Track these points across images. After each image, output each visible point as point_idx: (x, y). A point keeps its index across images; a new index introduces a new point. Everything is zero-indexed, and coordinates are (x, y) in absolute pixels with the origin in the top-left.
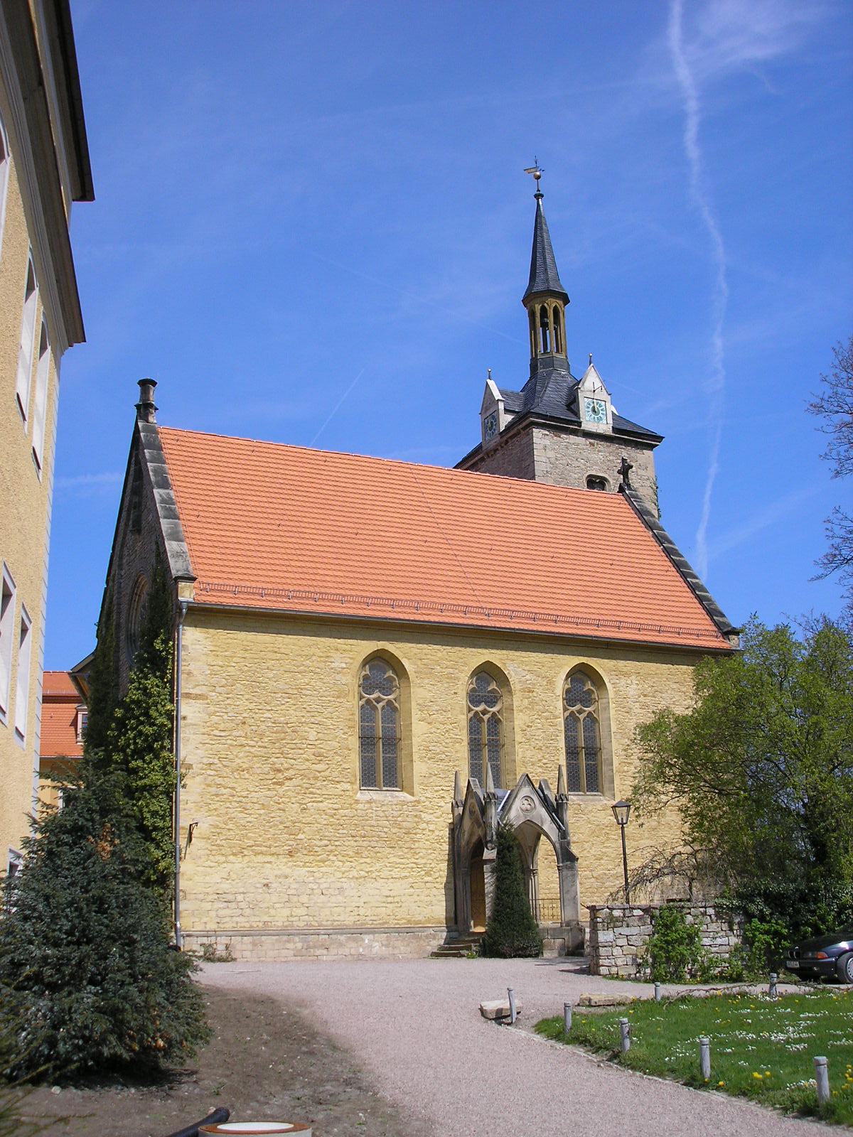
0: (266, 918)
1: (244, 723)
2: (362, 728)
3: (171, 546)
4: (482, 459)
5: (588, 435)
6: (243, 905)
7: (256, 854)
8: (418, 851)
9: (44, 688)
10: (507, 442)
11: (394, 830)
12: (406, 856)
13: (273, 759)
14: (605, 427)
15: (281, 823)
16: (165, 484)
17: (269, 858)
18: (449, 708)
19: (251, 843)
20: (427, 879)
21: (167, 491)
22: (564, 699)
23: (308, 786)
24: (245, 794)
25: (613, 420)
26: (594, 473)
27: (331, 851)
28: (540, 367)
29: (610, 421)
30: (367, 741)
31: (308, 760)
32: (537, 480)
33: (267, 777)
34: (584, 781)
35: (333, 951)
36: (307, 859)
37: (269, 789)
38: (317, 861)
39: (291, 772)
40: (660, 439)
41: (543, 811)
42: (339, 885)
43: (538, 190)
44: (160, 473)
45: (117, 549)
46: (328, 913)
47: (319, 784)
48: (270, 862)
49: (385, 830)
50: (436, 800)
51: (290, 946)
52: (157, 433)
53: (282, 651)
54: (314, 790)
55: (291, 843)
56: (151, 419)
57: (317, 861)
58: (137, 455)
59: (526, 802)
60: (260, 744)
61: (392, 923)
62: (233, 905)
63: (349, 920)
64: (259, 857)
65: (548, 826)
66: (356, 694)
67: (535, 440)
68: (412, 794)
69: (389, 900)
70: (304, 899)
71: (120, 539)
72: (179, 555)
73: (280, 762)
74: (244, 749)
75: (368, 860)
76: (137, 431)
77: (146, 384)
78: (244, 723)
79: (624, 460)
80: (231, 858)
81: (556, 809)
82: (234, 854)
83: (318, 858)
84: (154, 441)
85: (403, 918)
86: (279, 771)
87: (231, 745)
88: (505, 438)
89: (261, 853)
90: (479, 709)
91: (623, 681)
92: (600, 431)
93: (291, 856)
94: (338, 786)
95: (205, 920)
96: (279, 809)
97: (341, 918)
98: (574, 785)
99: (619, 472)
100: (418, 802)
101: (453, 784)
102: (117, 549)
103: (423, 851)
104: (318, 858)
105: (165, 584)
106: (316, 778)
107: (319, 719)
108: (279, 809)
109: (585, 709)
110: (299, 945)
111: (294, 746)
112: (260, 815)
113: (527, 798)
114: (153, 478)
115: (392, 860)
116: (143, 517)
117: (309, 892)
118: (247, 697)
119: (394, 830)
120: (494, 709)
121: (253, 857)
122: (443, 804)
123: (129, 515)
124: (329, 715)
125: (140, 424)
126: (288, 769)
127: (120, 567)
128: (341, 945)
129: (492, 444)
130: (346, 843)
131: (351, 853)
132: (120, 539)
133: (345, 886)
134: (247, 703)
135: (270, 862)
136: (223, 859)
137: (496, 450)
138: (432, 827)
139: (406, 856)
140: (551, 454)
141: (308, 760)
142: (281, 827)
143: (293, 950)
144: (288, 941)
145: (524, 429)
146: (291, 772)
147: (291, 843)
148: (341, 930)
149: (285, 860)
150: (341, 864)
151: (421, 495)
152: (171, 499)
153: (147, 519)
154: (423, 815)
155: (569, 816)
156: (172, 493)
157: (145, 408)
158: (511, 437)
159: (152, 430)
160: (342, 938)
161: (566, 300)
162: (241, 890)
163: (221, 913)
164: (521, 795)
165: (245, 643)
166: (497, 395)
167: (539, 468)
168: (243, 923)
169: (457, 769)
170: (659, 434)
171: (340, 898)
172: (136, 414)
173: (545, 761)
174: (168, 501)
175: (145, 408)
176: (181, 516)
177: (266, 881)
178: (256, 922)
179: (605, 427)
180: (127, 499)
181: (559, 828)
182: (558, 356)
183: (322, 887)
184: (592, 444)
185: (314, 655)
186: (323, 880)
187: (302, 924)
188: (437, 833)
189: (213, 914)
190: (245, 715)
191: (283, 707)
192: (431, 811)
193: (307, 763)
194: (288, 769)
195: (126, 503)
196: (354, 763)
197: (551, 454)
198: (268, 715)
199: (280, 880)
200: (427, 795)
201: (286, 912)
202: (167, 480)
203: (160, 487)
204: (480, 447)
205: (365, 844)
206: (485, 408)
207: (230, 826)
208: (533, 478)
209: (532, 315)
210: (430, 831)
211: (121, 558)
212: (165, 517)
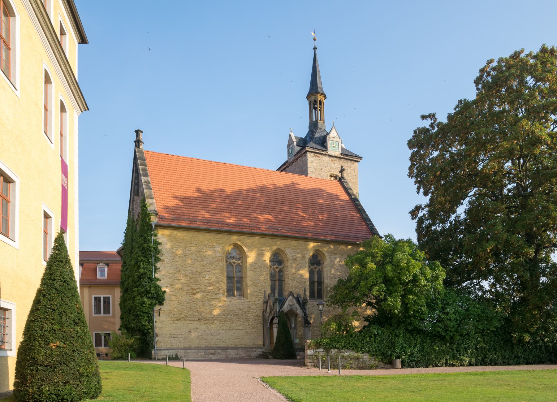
0: (190, 344)
1: (180, 271)
2: (227, 272)
3: (148, 201)
4: (287, 167)
5: (330, 156)
6: (181, 339)
7: (186, 320)
8: (249, 319)
9: (79, 249)
10: (297, 159)
11: (240, 312)
12: (245, 321)
13: (191, 285)
14: (338, 153)
15: (195, 309)
16: (146, 175)
17: (191, 322)
18: (262, 266)
19: (183, 316)
20: (253, 330)
21: (147, 178)
22: (309, 263)
23: (205, 295)
24: (180, 298)
25: (342, 150)
26: (332, 173)
27: (215, 319)
28: (314, 126)
29: (340, 150)
30: (230, 278)
31: (205, 285)
32: (309, 175)
33: (189, 292)
34: (316, 295)
35: (216, 356)
36: (205, 322)
37: (190, 296)
38: (209, 323)
39: (198, 290)
40: (361, 158)
41: (297, 306)
42: (218, 332)
43: (315, 46)
44: (145, 170)
45: (131, 202)
46: (214, 342)
47: (210, 294)
48: (191, 323)
49: (237, 312)
50: (257, 301)
51: (200, 354)
52: (143, 153)
53: (194, 243)
54: (208, 297)
55: (199, 316)
56: (141, 147)
57: (209, 323)
58: (136, 163)
59: (291, 302)
60: (186, 279)
61: (239, 346)
62: (177, 339)
63: (223, 345)
64: (187, 321)
65: (299, 311)
66: (225, 260)
67: (308, 159)
68: (247, 298)
69: (238, 337)
70: (205, 337)
71: (132, 198)
72: (151, 204)
73: (194, 286)
74: (180, 281)
75: (230, 323)
76: (135, 153)
77: (138, 132)
78: (180, 271)
79: (342, 167)
80: (176, 322)
81: (303, 305)
82: (177, 320)
83: (210, 322)
84: (142, 157)
85: (243, 344)
86: (194, 289)
87: (174, 279)
88: (296, 158)
89: (188, 320)
90: (275, 267)
91: (333, 256)
92: (336, 155)
93: (200, 321)
94: (218, 295)
95: (166, 344)
96: (194, 304)
97: (219, 344)
98: (312, 296)
99: (340, 172)
100: (250, 302)
101: (263, 295)
102: (131, 202)
103: (252, 320)
104: (210, 322)
105: (145, 214)
106: (209, 292)
107: (209, 270)
108: (194, 304)
109: (318, 267)
110: (203, 354)
111: (199, 280)
112: (187, 306)
113: (291, 300)
114: (141, 172)
115: (239, 323)
116: (139, 189)
117: (207, 334)
118: (180, 261)
119: (240, 312)
120: (281, 267)
121: (184, 322)
122: (259, 302)
123: (134, 188)
124: (213, 268)
125: (136, 150)
126: (197, 289)
127: (133, 209)
128: (219, 353)
129: (292, 160)
130: (221, 317)
131: (223, 320)
132: (132, 198)
133: (221, 332)
134: (180, 263)
135: (191, 323)
136: (173, 322)
137: (293, 163)
138: (254, 311)
139: (245, 321)
140: (315, 165)
141: (205, 285)
142: (195, 310)
143: (200, 355)
144: (199, 352)
145: (304, 153)
146: (198, 290)
147: (199, 316)
148: (220, 348)
149: (197, 323)
150: (219, 324)
151: (254, 180)
152: (149, 181)
153: (141, 189)
154: (251, 306)
155: (307, 307)
156: (149, 179)
157: (138, 143)
158: (299, 157)
159: (142, 152)
160: (220, 351)
161: (325, 98)
162: (180, 333)
163: (172, 342)
164: (289, 299)
165: (179, 240)
166: (294, 139)
167: (310, 170)
168: (181, 345)
169: (265, 289)
170: (361, 156)
171: (219, 337)
172: (134, 145)
173: (300, 287)
174: (147, 182)
175: (138, 143)
176: (153, 188)
177: (189, 330)
178: (186, 345)
179: (338, 153)
180: (133, 181)
181: (303, 311)
182: (320, 122)
183: (212, 332)
184: (332, 160)
185: (207, 245)
186: (212, 330)
187: (204, 346)
188: (257, 313)
189: (169, 342)
190: (180, 268)
191: (195, 265)
192: (255, 305)
193: (205, 286)
194: (197, 289)
195: (133, 183)
196: (224, 286)
197: (315, 165)
198: (189, 268)
199: (195, 330)
200: (253, 299)
201: (198, 341)
202: (147, 173)
203: (144, 176)
204: (287, 162)
205: (228, 317)
206: (289, 146)
207: (175, 310)
208: (307, 175)
209: (310, 103)
210: (254, 312)
211: (133, 206)
212: (146, 189)
